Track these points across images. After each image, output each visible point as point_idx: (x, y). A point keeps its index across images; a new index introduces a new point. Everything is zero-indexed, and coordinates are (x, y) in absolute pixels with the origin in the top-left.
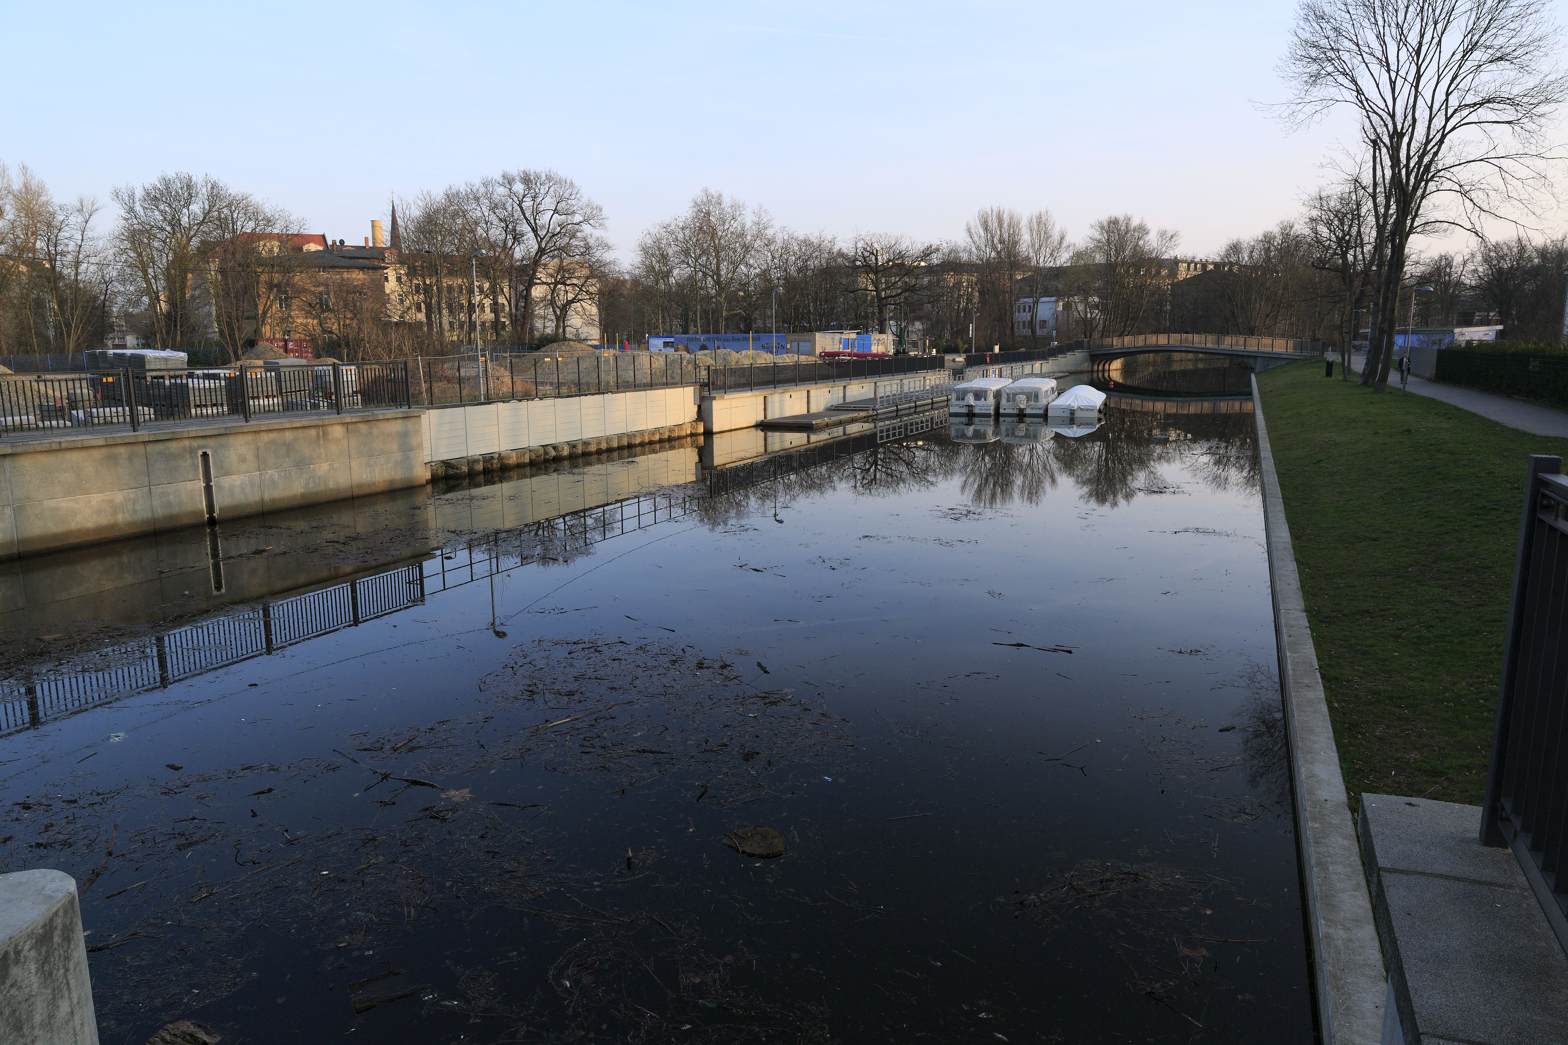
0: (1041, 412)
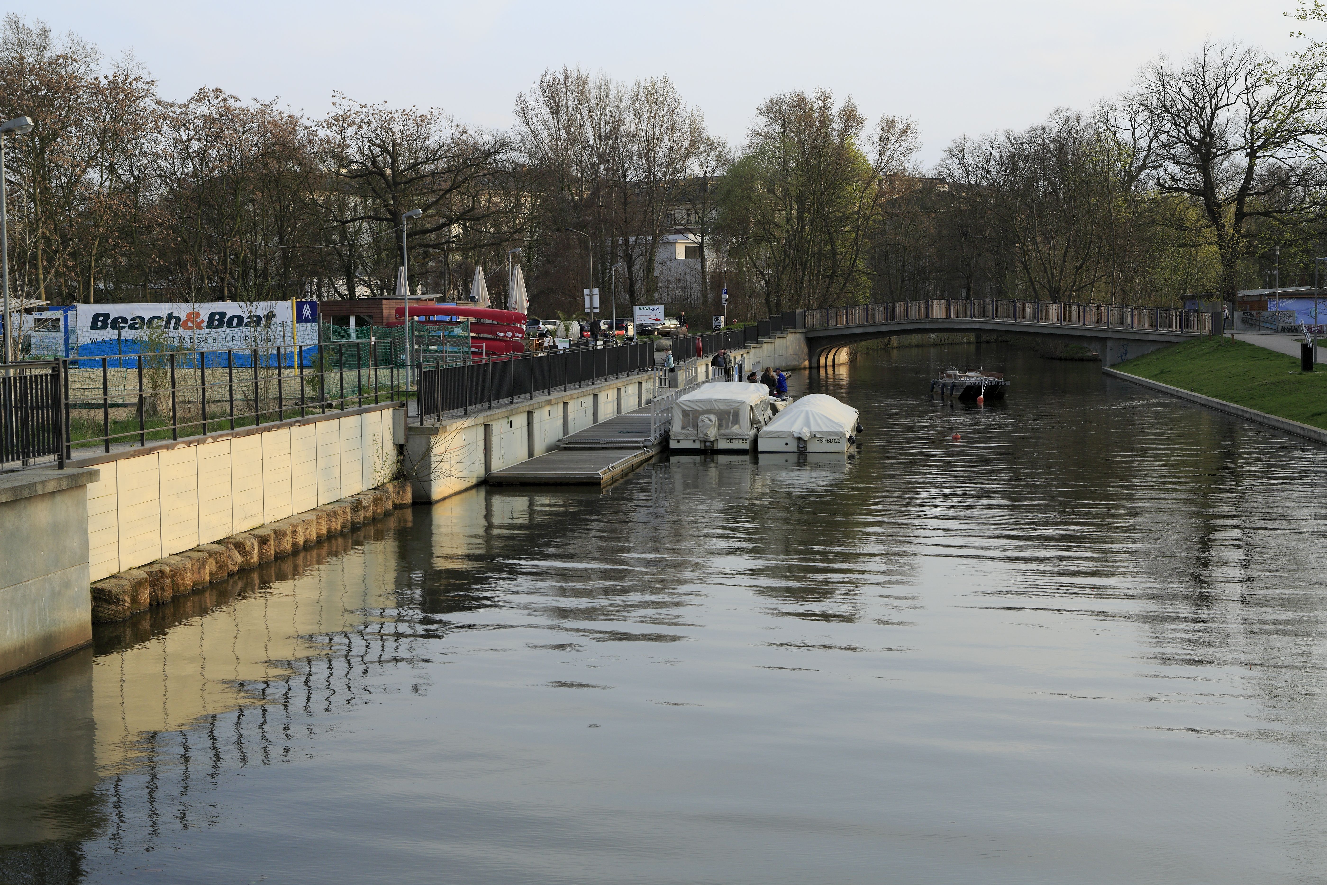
0: (746, 446)
